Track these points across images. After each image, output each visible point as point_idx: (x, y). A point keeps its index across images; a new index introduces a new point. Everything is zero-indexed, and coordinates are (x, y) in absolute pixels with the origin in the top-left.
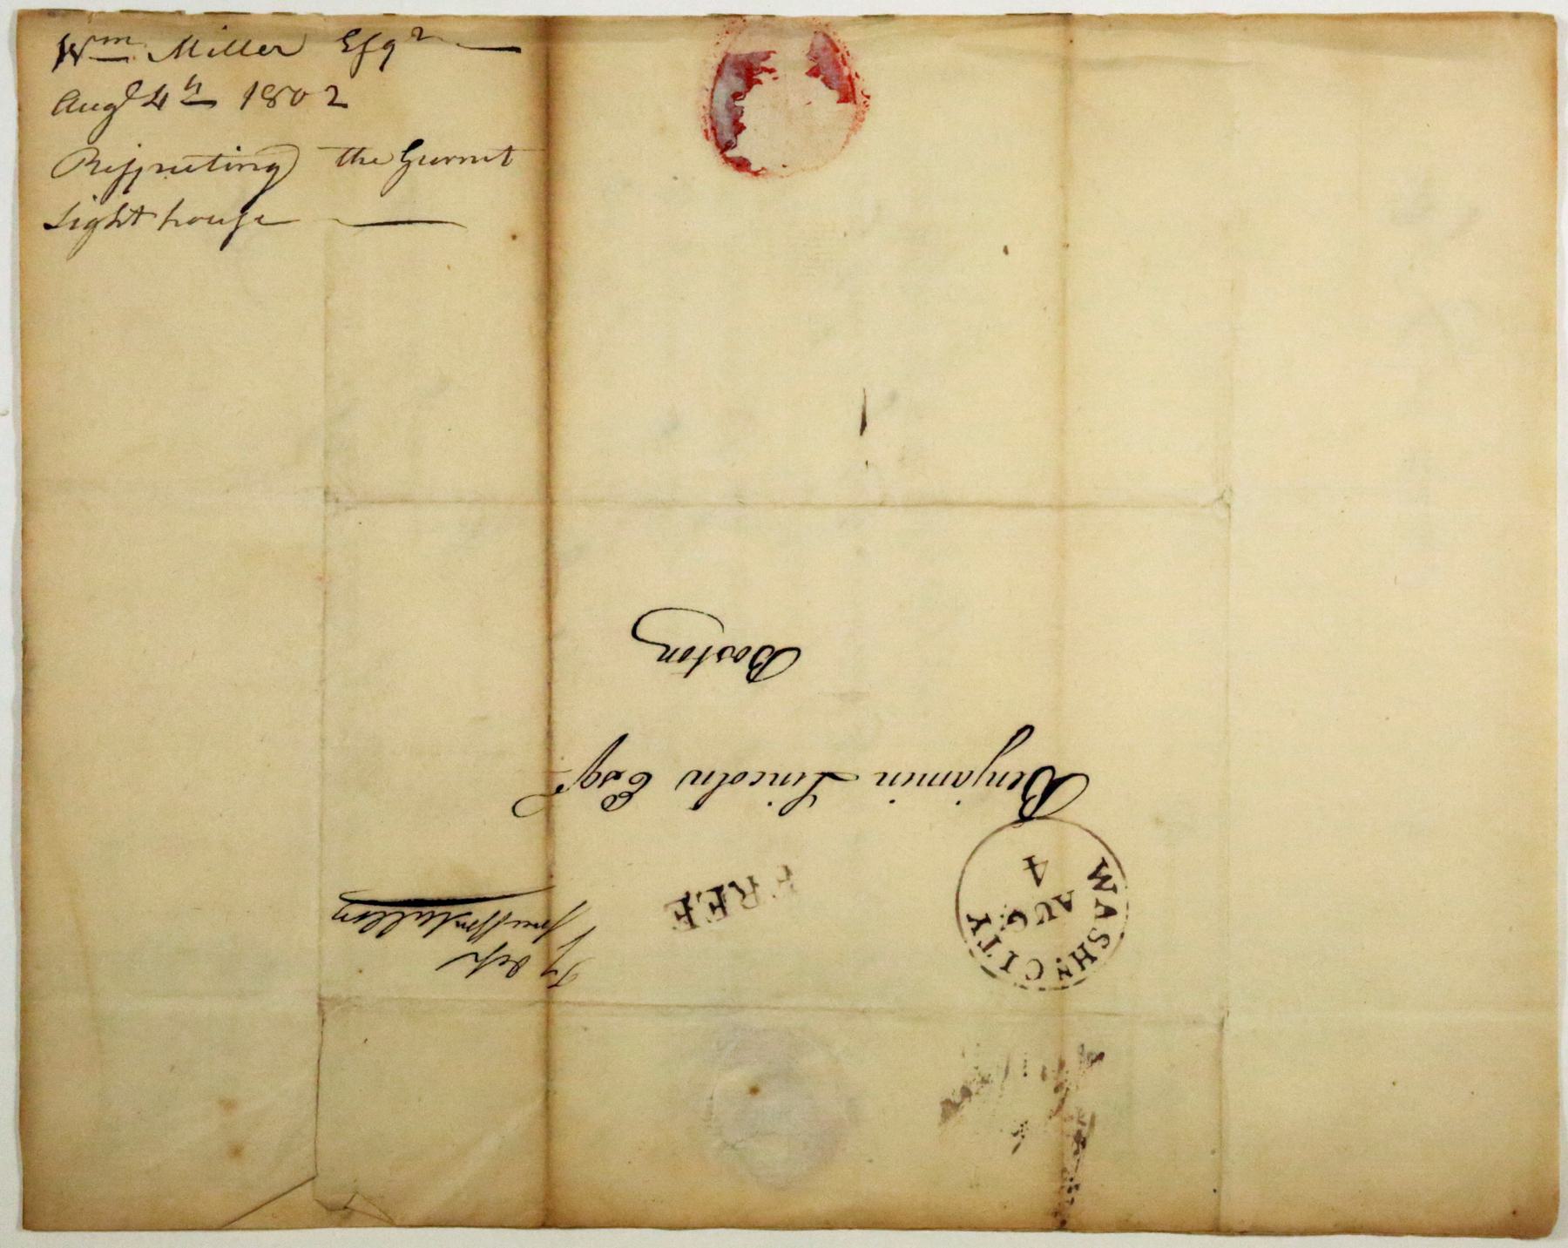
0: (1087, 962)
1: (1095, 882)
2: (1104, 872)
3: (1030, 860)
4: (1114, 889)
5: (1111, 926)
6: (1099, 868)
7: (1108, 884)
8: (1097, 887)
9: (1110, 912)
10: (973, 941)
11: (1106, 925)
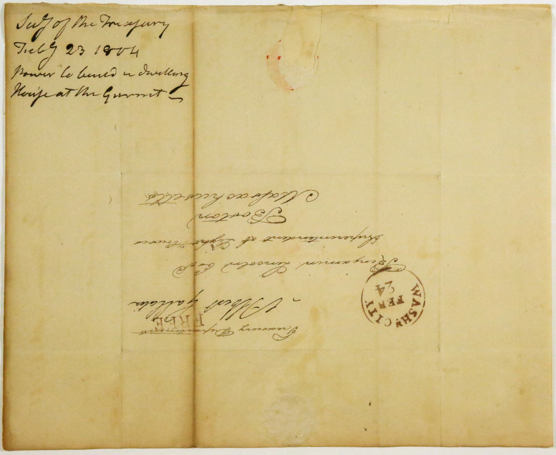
0: (408, 321)
1: (414, 292)
2: (417, 289)
3: (378, 286)
4: (420, 295)
5: (418, 309)
6: (415, 287)
7: (418, 293)
8: (415, 294)
9: (418, 304)
10: (366, 310)
11: (416, 308)
